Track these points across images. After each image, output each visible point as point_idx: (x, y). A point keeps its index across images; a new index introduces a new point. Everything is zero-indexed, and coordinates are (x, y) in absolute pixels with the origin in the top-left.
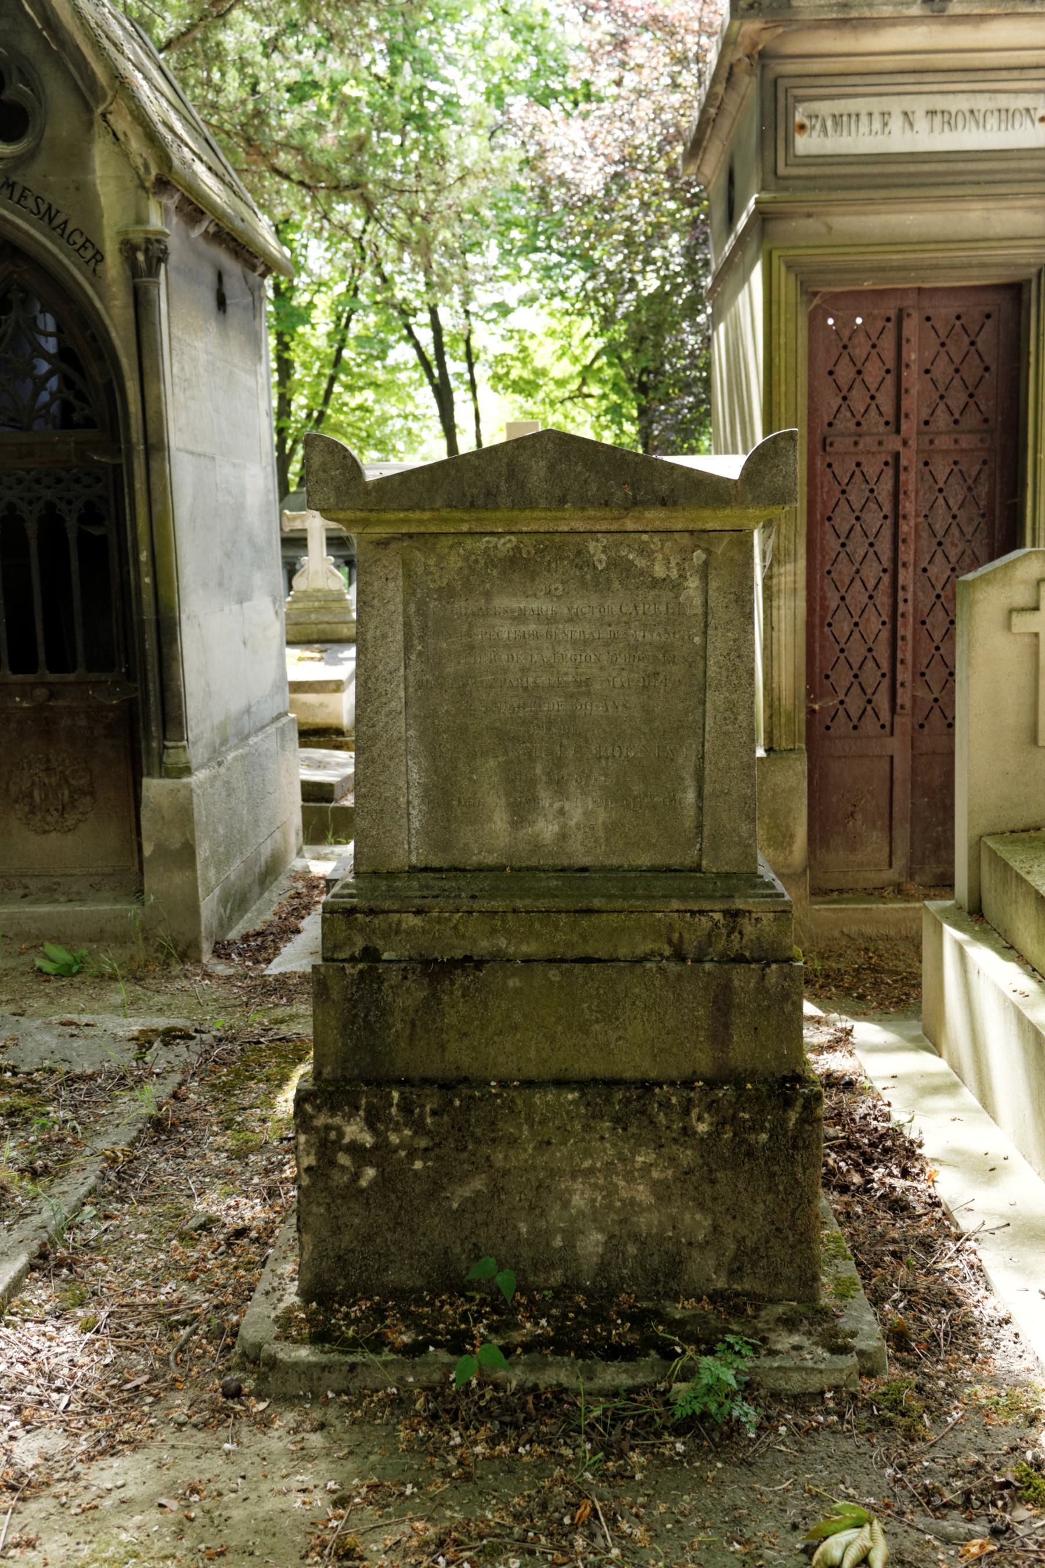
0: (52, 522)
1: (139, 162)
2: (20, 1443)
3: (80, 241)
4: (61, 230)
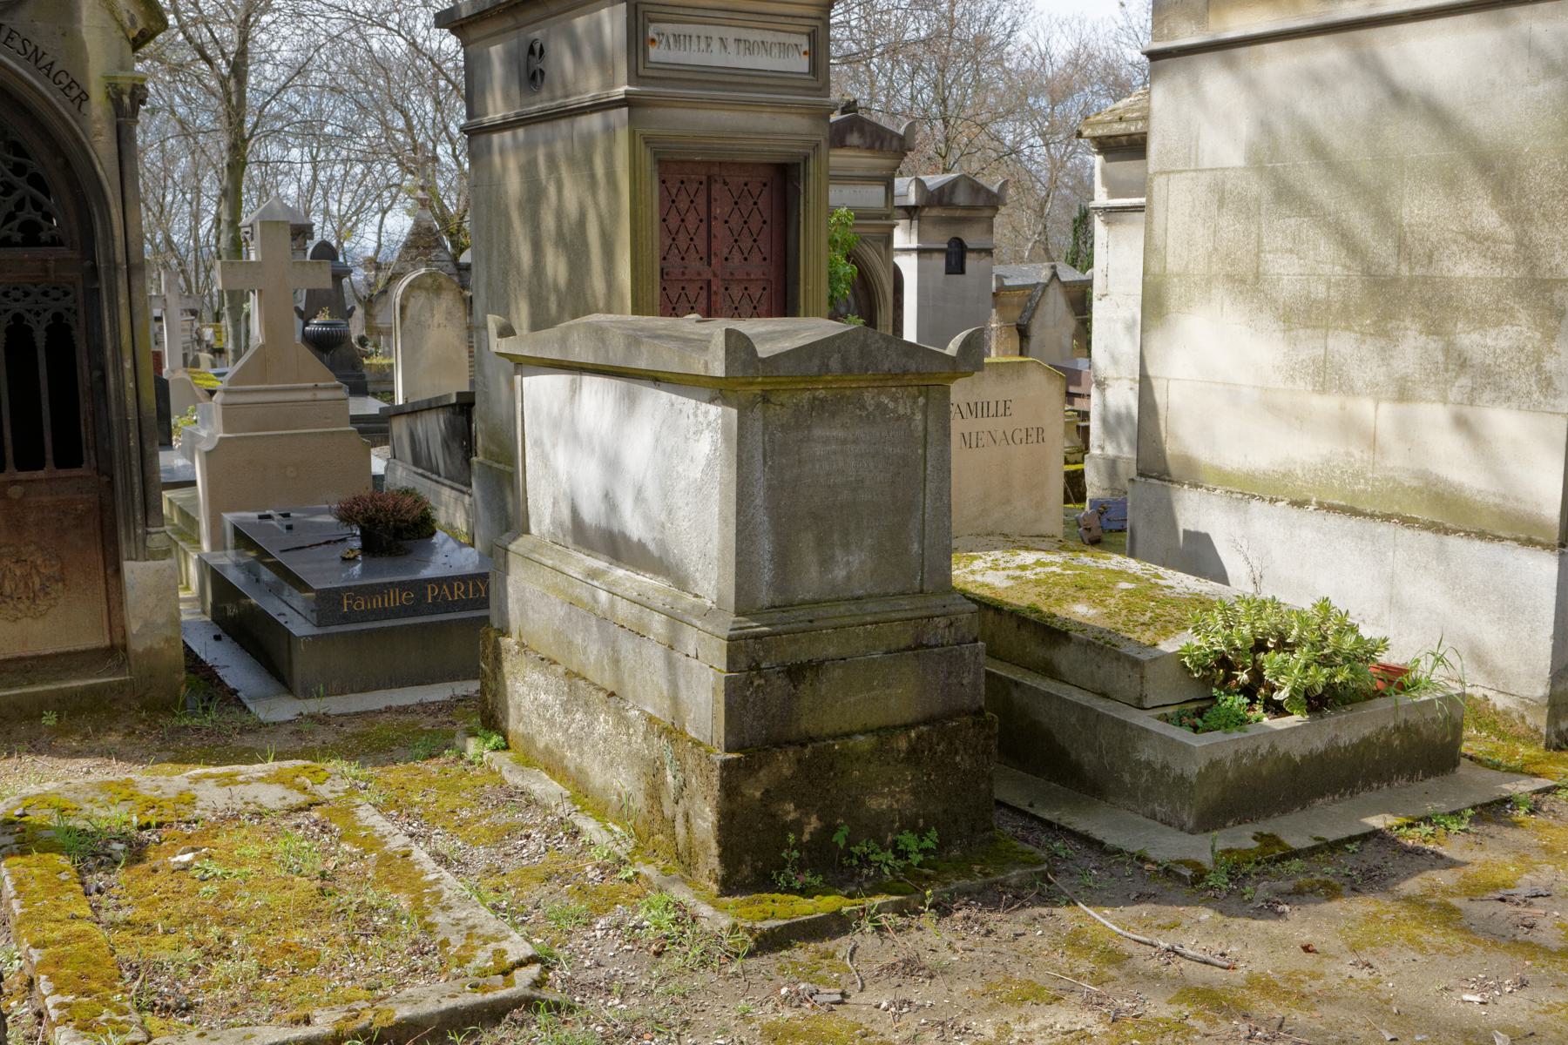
1: (125, 16)
3: (66, 81)
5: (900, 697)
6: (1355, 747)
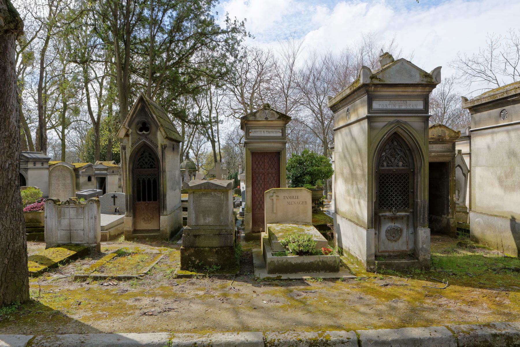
0: (149, 181)
2: (225, 124)
4: (153, 143)
5: (215, 242)
6: (309, 264)
